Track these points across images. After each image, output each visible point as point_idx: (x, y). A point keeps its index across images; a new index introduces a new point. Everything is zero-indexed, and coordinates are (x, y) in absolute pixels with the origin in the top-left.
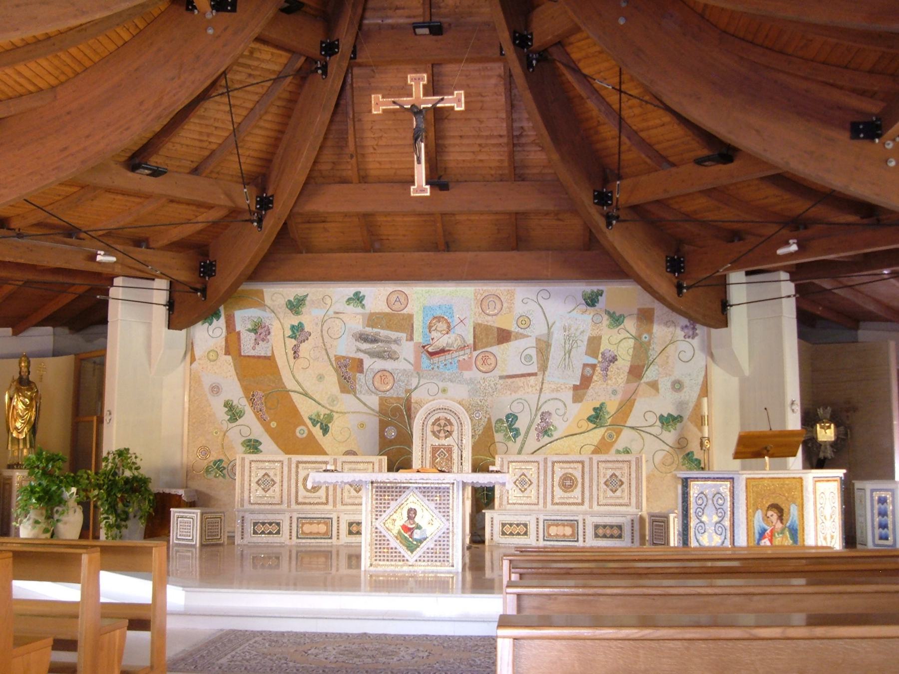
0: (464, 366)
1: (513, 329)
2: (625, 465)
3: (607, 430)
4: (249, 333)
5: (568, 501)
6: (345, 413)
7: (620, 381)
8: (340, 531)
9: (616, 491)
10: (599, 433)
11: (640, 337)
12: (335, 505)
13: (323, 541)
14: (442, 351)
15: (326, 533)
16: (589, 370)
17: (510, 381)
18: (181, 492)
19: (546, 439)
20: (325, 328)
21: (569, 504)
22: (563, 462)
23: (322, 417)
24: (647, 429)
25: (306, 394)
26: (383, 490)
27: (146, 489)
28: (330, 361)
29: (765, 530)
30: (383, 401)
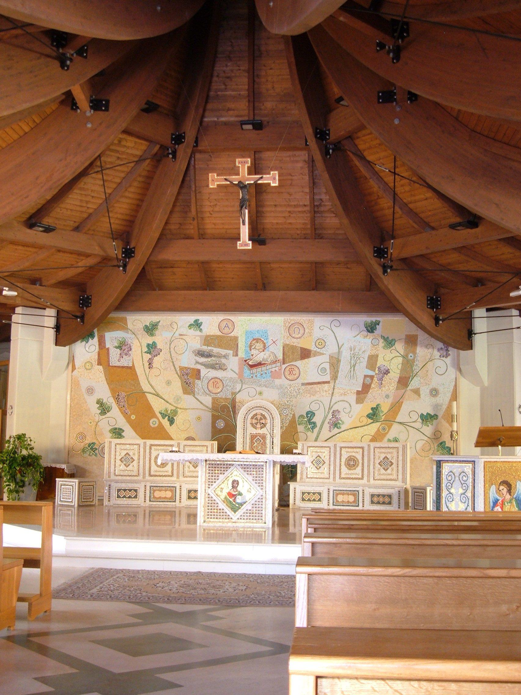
0: (276, 375)
1: (312, 349)
2: (394, 451)
3: (382, 424)
4: (115, 349)
5: (351, 477)
6: (187, 409)
7: (391, 388)
8: (182, 496)
9: (387, 469)
10: (374, 427)
11: (407, 356)
12: (178, 477)
13: (169, 503)
14: (260, 364)
15: (171, 498)
16: (368, 380)
17: (309, 387)
18: (64, 466)
19: (336, 431)
20: (172, 346)
21: (352, 479)
22: (348, 447)
23: (169, 412)
24: (411, 424)
25: (158, 395)
26: (214, 466)
27: (38, 464)
28: (176, 370)
29: (498, 500)
30: (214, 400)
